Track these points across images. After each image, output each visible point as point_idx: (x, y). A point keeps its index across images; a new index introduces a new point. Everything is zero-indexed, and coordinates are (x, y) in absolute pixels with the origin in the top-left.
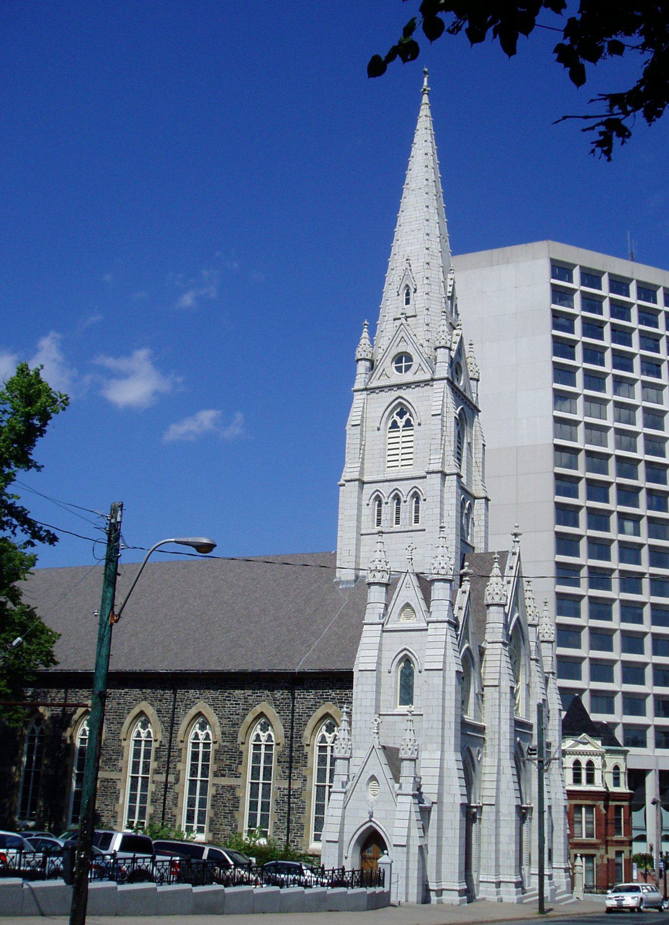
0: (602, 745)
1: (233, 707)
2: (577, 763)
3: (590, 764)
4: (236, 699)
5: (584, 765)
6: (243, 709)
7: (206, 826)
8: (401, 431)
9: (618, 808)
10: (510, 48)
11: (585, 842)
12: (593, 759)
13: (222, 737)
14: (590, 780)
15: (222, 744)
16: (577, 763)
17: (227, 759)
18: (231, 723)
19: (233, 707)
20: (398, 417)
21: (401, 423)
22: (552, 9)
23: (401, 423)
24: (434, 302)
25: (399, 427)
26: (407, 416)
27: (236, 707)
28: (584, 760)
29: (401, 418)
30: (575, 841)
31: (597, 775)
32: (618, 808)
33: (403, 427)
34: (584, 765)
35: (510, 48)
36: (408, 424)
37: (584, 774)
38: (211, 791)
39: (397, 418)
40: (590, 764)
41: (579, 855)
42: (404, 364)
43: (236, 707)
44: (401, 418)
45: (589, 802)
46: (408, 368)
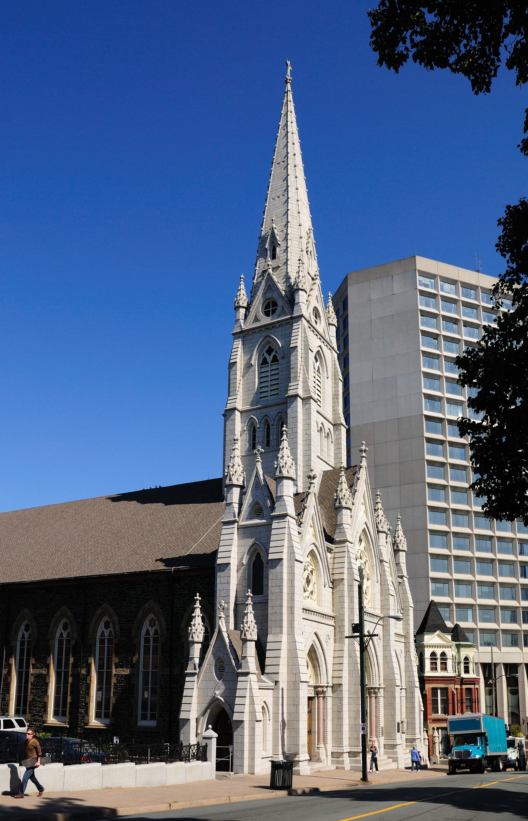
0: (453, 640)
1: (128, 606)
2: (433, 654)
3: (443, 654)
4: (130, 599)
5: (438, 656)
6: (135, 607)
7: (157, 713)
8: (270, 365)
9: (435, 690)
10: (397, 71)
11: (440, 717)
12: (446, 650)
13: (121, 633)
14: (444, 668)
15: (120, 639)
16: (433, 654)
17: (124, 652)
18: (127, 620)
19: (128, 606)
20: (267, 354)
21: (269, 359)
22: (490, 86)
23: (269, 359)
24: (294, 255)
25: (268, 363)
26: (273, 353)
27: (130, 606)
28: (439, 652)
29: (270, 355)
30: (433, 717)
31: (449, 663)
32: (435, 690)
33: (271, 362)
34: (438, 656)
35: (397, 71)
36: (275, 359)
37: (439, 662)
38: (31, 679)
39: (266, 355)
40: (443, 654)
41: (436, 728)
42: (271, 309)
43: (130, 606)
44: (270, 355)
45: (443, 686)
46: (274, 311)
